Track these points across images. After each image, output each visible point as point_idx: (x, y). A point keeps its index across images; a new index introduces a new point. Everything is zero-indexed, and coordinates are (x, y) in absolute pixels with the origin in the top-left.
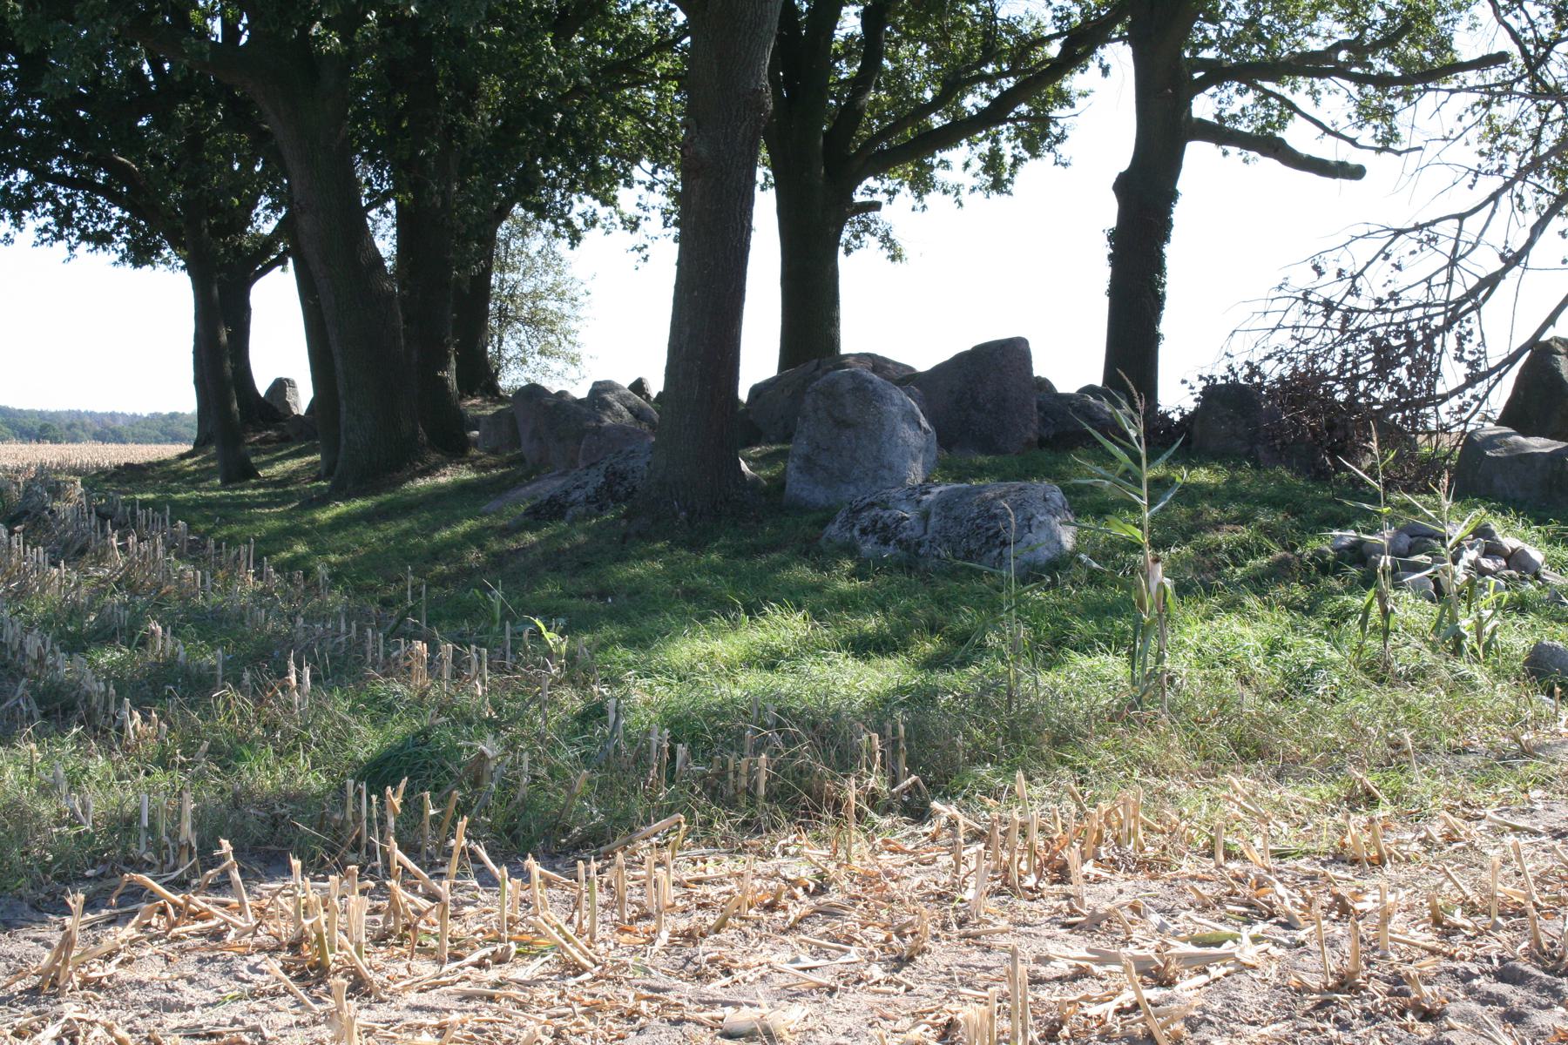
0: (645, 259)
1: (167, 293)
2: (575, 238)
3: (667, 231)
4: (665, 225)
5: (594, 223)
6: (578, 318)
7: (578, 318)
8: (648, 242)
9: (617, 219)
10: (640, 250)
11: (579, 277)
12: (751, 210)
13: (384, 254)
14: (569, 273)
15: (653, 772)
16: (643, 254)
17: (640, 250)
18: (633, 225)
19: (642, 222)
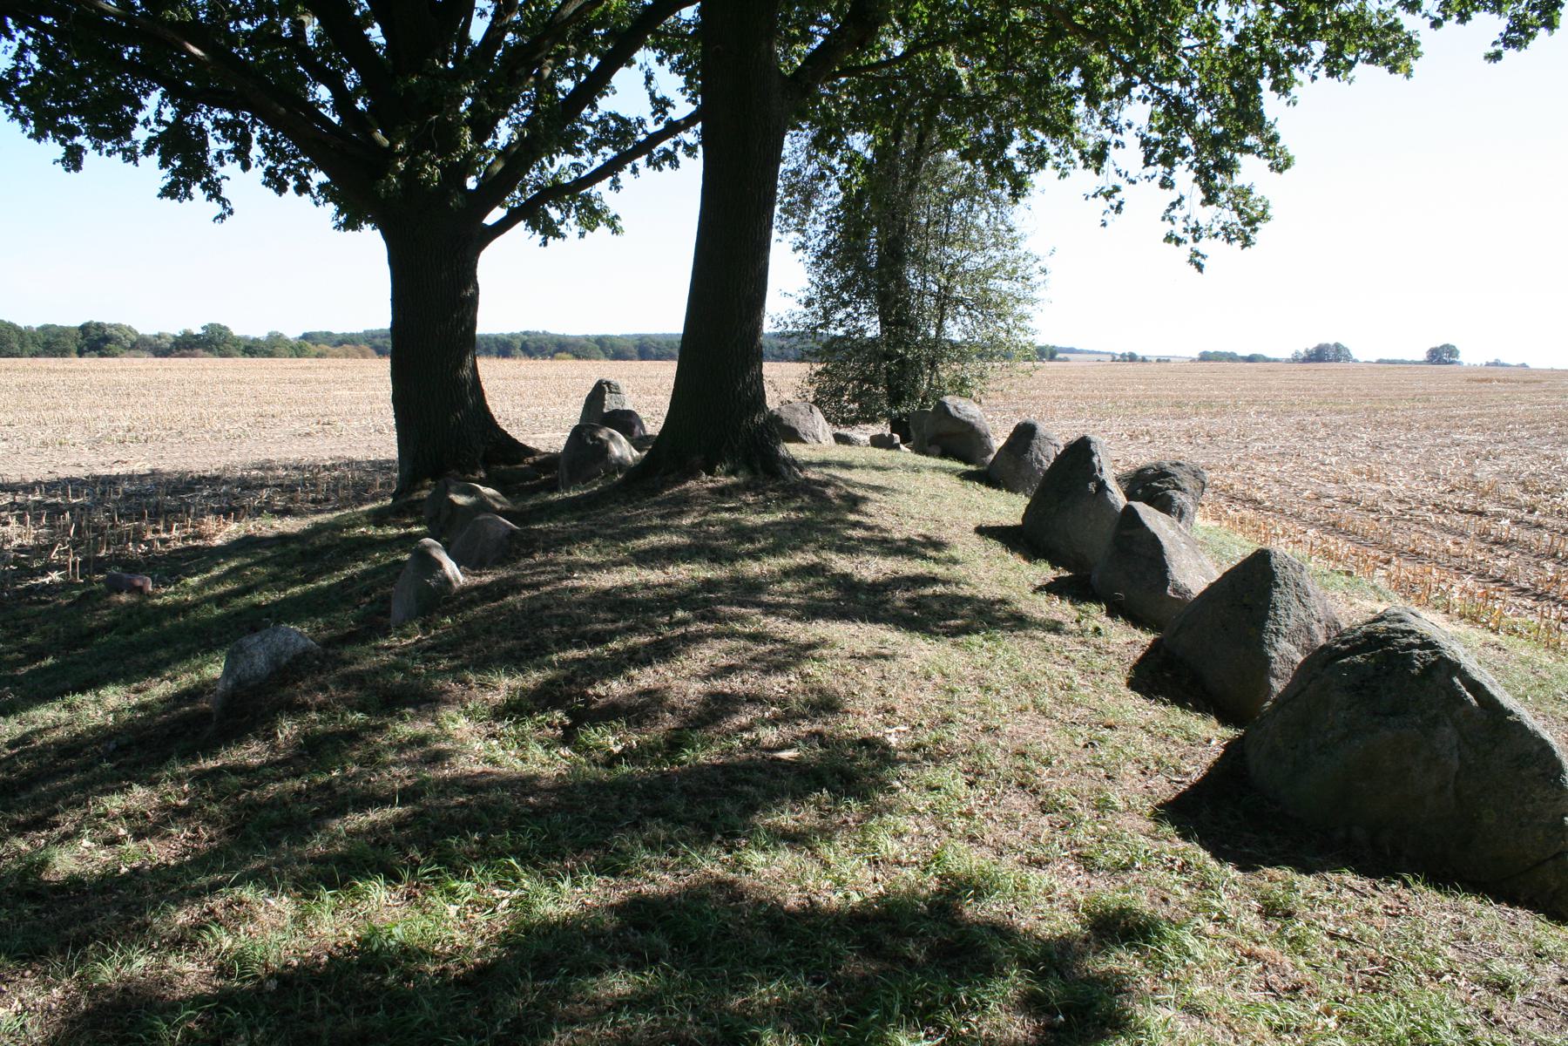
0: (1118, 209)
1: (345, 275)
2: (1019, 187)
3: (1150, 170)
4: (1147, 163)
5: (1041, 163)
6: (1033, 302)
7: (1033, 302)
8: (1121, 182)
9: (1075, 154)
10: (1109, 195)
11: (1036, 252)
12: (475, 266)
13: (1277, 666)
14: (1023, 247)
15: (123, 377)
16: (1114, 202)
17: (1109, 195)
18: (1098, 157)
19: (1111, 150)
